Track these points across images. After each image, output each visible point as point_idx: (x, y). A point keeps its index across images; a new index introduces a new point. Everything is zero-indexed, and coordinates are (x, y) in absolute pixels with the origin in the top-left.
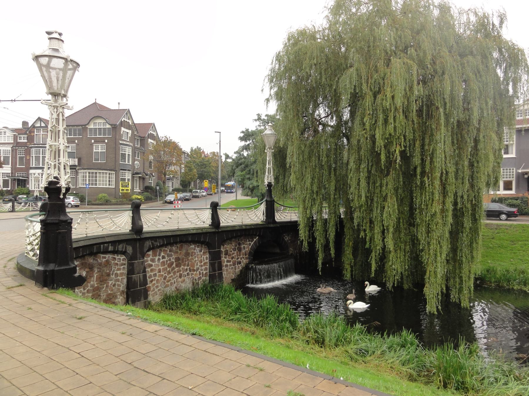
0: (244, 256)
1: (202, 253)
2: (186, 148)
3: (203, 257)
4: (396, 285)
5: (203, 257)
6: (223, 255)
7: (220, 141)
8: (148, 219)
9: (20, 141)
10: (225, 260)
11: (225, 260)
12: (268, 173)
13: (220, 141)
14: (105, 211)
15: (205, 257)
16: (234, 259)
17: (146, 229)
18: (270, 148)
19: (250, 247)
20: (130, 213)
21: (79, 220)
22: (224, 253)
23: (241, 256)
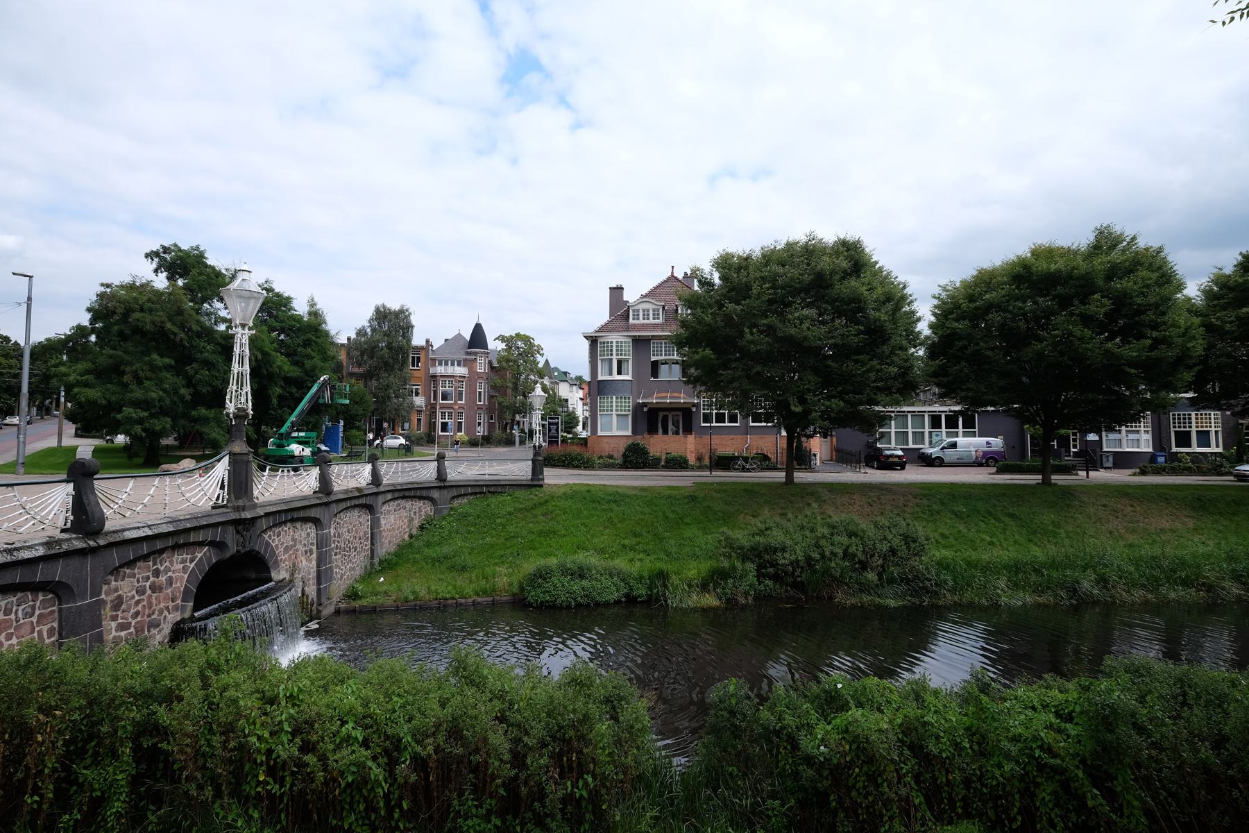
0: (171, 604)
1: (34, 619)
2: (85, 319)
3: (40, 633)
4: (997, 443)
5: (40, 633)
6: (107, 611)
7: (29, 299)
8: (110, 497)
9: (636, 322)
10: (114, 624)
11: (114, 624)
12: (237, 383)
13: (29, 299)
14: (8, 485)
15: (45, 629)
16: (139, 619)
17: (449, 477)
18: (243, 326)
19: (186, 576)
20: (70, 488)
21: (153, 489)
22: (109, 606)
23: (162, 605)
